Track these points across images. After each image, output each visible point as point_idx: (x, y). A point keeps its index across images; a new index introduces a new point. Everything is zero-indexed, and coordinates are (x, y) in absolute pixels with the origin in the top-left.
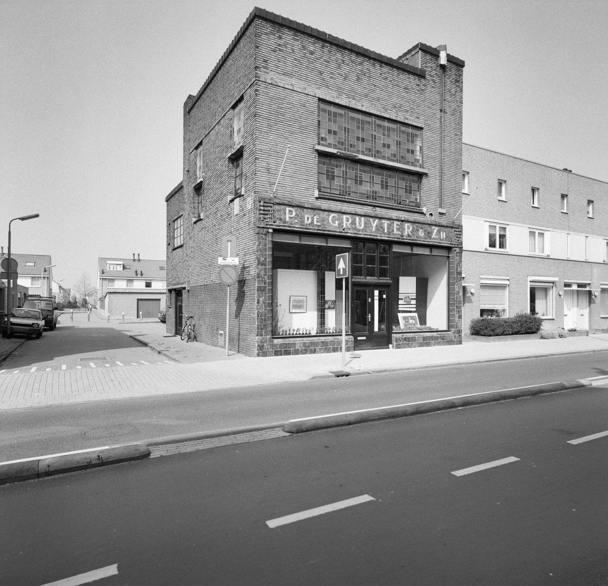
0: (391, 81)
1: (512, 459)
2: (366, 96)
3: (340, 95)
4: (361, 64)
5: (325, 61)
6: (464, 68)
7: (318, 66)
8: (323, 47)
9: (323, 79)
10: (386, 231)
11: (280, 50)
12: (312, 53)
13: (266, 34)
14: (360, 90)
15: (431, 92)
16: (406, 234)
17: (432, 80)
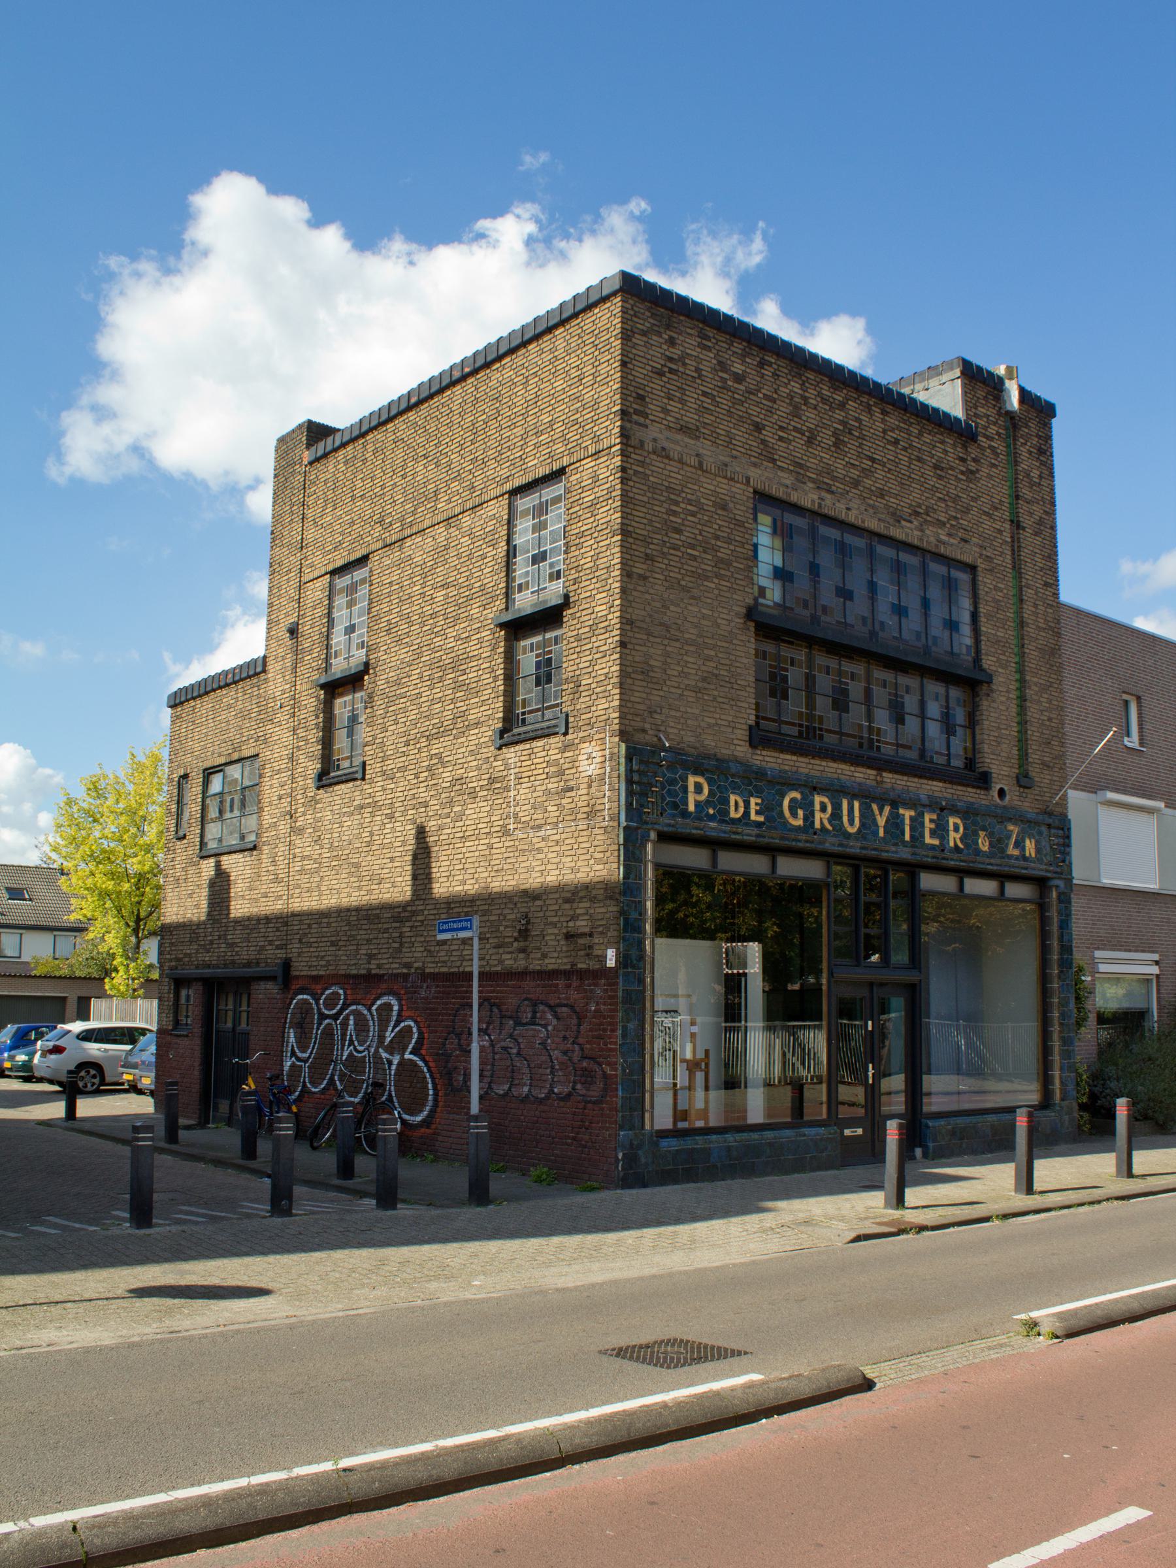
0: (905, 449)
1: (1132, 1514)
2: (856, 484)
3: (801, 479)
4: (842, 406)
5: (766, 397)
6: (1054, 421)
7: (754, 410)
8: (762, 364)
9: (763, 442)
10: (907, 837)
11: (671, 371)
12: (739, 378)
13: (644, 333)
14: (839, 467)
15: (990, 477)
16: (952, 844)
17: (990, 447)
